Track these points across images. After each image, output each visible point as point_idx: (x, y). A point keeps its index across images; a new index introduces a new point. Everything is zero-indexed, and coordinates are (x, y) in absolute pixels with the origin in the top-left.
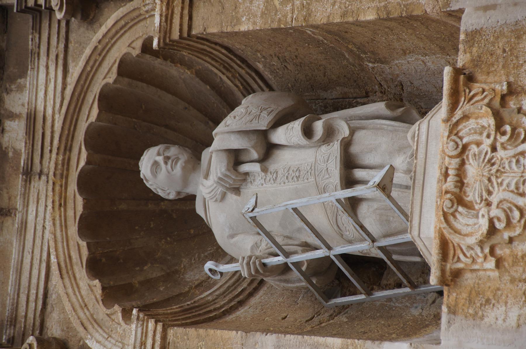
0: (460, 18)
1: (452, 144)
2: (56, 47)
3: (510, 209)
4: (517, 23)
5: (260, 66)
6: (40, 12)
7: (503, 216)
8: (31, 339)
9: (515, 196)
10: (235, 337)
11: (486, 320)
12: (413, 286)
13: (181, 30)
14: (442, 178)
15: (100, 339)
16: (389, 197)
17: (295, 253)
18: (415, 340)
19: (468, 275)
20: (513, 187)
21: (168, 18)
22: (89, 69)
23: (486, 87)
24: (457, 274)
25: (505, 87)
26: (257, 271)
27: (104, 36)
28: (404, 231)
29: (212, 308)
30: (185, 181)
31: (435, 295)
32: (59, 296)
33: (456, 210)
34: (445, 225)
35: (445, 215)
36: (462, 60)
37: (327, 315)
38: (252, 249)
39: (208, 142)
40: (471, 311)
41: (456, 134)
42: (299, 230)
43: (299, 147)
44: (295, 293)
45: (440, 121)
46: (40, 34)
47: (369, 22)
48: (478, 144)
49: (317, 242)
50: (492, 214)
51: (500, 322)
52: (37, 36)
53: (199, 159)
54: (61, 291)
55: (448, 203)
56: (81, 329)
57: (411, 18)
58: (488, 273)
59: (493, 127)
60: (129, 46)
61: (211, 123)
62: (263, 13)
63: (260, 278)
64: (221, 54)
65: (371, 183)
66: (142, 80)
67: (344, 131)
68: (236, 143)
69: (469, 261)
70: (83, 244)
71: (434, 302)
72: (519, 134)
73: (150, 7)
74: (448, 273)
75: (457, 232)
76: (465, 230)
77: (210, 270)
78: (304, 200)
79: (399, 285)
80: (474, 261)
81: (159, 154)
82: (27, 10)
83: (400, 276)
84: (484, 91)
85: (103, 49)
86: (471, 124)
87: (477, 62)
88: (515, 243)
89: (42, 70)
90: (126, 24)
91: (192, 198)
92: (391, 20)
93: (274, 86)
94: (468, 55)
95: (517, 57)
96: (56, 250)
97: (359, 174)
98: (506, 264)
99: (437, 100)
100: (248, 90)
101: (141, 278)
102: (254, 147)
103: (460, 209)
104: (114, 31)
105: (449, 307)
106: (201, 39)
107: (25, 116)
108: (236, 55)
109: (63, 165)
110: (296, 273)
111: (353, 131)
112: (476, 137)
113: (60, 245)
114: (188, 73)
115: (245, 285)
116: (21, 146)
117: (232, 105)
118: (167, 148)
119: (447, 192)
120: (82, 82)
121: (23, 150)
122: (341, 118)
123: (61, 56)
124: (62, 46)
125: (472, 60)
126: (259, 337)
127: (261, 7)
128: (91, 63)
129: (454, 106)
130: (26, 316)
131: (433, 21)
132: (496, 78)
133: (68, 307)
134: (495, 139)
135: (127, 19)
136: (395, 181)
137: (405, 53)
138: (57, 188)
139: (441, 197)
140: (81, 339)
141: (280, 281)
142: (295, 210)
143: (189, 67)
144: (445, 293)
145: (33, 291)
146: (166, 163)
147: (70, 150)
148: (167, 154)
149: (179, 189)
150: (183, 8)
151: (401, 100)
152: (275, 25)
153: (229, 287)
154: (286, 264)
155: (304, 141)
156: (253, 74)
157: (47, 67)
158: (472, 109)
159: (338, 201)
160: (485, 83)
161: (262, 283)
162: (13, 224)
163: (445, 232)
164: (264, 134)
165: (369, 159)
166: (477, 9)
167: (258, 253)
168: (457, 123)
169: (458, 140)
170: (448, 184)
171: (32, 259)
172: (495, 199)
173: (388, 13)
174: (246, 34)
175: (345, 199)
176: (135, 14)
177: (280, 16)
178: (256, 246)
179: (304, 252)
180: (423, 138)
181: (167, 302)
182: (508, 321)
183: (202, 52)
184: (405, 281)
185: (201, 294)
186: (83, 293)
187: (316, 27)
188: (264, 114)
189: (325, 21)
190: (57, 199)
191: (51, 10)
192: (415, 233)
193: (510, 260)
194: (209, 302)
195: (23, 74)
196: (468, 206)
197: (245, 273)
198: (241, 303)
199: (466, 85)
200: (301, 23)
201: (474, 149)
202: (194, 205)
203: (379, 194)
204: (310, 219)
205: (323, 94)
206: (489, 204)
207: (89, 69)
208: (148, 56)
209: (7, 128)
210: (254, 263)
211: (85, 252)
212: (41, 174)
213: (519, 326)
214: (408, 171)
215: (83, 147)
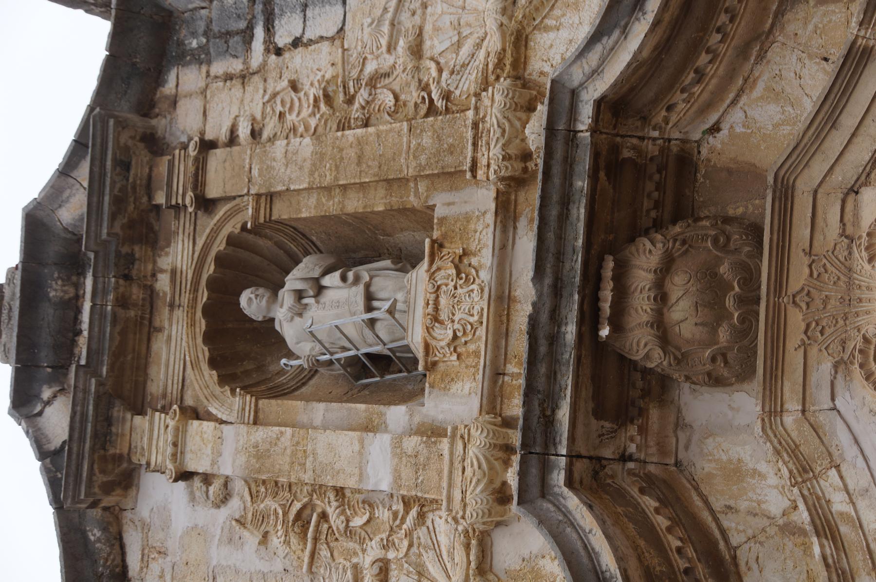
0: (434, 210)
1: (431, 285)
2: (189, 228)
3: (465, 324)
4: (467, 213)
5: (314, 238)
6: (179, 208)
7: (461, 328)
8: (175, 407)
9: (468, 316)
10: (299, 404)
11: (451, 391)
12: (409, 372)
13: (265, 217)
14: (425, 306)
15: (217, 406)
16: (394, 318)
17: (337, 353)
18: (409, 404)
19: (441, 364)
20: (467, 311)
21: (257, 210)
22: (208, 241)
23: (451, 251)
24: (435, 364)
25: (461, 251)
26: (313, 364)
27: (218, 221)
28: (403, 339)
29: (286, 387)
30: (269, 309)
31: (422, 376)
32: (191, 381)
33: (434, 325)
34: (427, 334)
35: (427, 328)
36: (436, 234)
37: (356, 390)
38: (310, 350)
39: (282, 285)
40: (443, 386)
41: (434, 279)
42: (339, 339)
43: (338, 288)
44: (336, 377)
45: (424, 271)
46: (179, 221)
47: (380, 212)
48: (446, 285)
49: (350, 346)
50: (455, 327)
51: (459, 391)
52: (177, 222)
53: (277, 295)
54: (193, 378)
55: (429, 321)
56: (205, 401)
57: (405, 209)
58: (453, 363)
59: (455, 275)
60: (233, 227)
61: (284, 274)
62: (315, 207)
63: (315, 368)
64: (290, 231)
65: (383, 310)
66: (241, 248)
67: (366, 277)
68: (299, 286)
69: (442, 356)
70: (206, 349)
71: (421, 381)
72: (470, 279)
73: (246, 203)
74: (429, 364)
75: (434, 338)
76: (439, 337)
77: (285, 364)
78: (342, 320)
79: (400, 371)
80: (444, 356)
81: (252, 293)
82: (171, 207)
83: (401, 366)
84: (449, 253)
85: (217, 229)
86: (442, 273)
87: (444, 236)
88: (468, 345)
89: (180, 243)
90: (232, 214)
91: (273, 320)
92: (393, 210)
93: (323, 251)
94: (439, 232)
95: (468, 233)
96: (189, 353)
97: (376, 304)
98: (463, 357)
99: (422, 259)
100: (307, 253)
101: (242, 370)
102: (311, 288)
103: (436, 324)
104: (224, 218)
105: (430, 384)
106: (277, 222)
107: (169, 271)
108: (299, 232)
109: (193, 300)
110: (337, 365)
111: (371, 278)
112: (445, 281)
113: (191, 349)
114: (269, 243)
115: (306, 373)
116: (167, 289)
117: (297, 262)
118: (257, 289)
119: (428, 314)
120: (204, 250)
121: (169, 292)
122: (364, 270)
123: (192, 234)
124: (192, 228)
125: (442, 235)
126: (315, 404)
127: (314, 202)
128: (210, 238)
129: (432, 262)
130: (172, 393)
131: (418, 211)
132: (456, 246)
133: (197, 387)
134: (456, 282)
135: (231, 211)
136: (397, 308)
137: (402, 230)
138: (190, 315)
139: (425, 317)
140: (205, 407)
141: (328, 370)
142: (336, 326)
143: (270, 240)
144: (428, 375)
145: (176, 378)
146: (256, 298)
147: (197, 291)
148: (257, 293)
149: (264, 314)
150: (266, 204)
151: (401, 259)
152: (323, 214)
153: (296, 374)
154: (331, 360)
155: (341, 284)
156: (310, 244)
157: (183, 241)
158: (443, 264)
159: (363, 320)
160: (450, 248)
161: (316, 371)
162: (163, 337)
163: (427, 338)
164: (317, 280)
165: (381, 295)
166: (444, 204)
167: (314, 353)
168: (434, 273)
169: (435, 283)
170: (429, 310)
171: (175, 358)
172: (456, 318)
173: (392, 206)
174: (305, 219)
175: (368, 319)
176: (236, 208)
177: (325, 208)
178: (313, 349)
179: (342, 352)
180: (414, 281)
181: (258, 384)
182: (464, 391)
183: (278, 230)
184: (404, 369)
185: (279, 378)
186: (206, 379)
187: (348, 215)
188: (317, 268)
189: (353, 211)
190: (189, 321)
191: (185, 206)
192: (410, 339)
193: (465, 354)
194: (284, 384)
195: (168, 245)
196: (441, 323)
197: (306, 366)
198: (304, 384)
199: (438, 249)
200: (339, 212)
201: (444, 288)
202: (274, 324)
203: (388, 316)
204: (346, 332)
205: (353, 255)
206: (453, 321)
207: (208, 241)
208: (245, 233)
209: (159, 278)
210: (312, 359)
211: (207, 354)
212: (179, 306)
213: (470, 394)
214: (405, 302)
215: (205, 290)
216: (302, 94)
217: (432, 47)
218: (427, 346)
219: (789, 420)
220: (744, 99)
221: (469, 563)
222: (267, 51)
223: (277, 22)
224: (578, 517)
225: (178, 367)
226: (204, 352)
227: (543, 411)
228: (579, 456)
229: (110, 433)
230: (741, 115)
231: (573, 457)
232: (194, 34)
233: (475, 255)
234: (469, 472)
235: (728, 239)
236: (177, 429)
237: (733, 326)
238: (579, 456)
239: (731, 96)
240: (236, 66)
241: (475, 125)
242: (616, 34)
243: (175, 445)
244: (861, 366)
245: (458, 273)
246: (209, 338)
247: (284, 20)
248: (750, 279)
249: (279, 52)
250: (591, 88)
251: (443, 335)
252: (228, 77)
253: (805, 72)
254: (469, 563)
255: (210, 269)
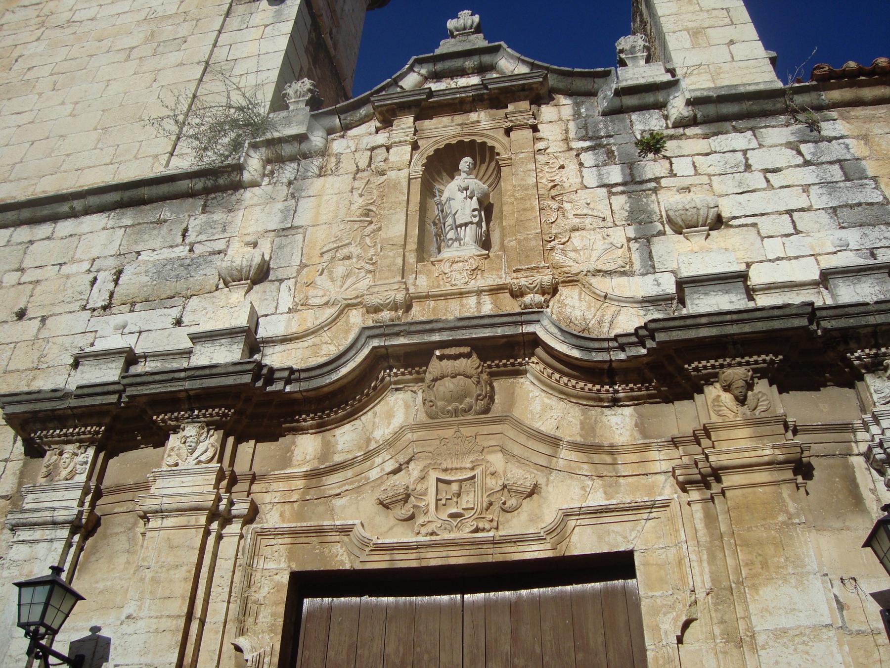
2: (497, 125)
30: (464, 172)
129: (478, 256)
216: (557, 172)
217: (575, 237)
218: (441, 261)
219: (409, 436)
220: (543, 394)
221: (351, 299)
222: (578, 149)
223: (591, 152)
224: (360, 355)
225: (435, 134)
226: (441, 146)
227: (402, 331)
228: (387, 349)
229: (404, 109)
230: (537, 394)
231: (385, 347)
232: (587, 110)
233: (482, 276)
234: (386, 293)
235: (482, 400)
236: (406, 141)
237: (446, 406)
238: (387, 349)
239: (545, 389)
240: (572, 135)
241: (537, 268)
242: (562, 339)
243: (400, 142)
244: (430, 463)
245: (473, 270)
246: (448, 146)
247: (592, 156)
248: (466, 411)
249: (578, 155)
250: (541, 329)
251: (446, 268)
252: (567, 131)
253: (553, 420)
254: (351, 299)
255: (479, 140)
